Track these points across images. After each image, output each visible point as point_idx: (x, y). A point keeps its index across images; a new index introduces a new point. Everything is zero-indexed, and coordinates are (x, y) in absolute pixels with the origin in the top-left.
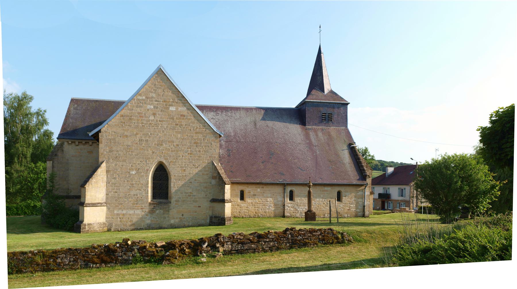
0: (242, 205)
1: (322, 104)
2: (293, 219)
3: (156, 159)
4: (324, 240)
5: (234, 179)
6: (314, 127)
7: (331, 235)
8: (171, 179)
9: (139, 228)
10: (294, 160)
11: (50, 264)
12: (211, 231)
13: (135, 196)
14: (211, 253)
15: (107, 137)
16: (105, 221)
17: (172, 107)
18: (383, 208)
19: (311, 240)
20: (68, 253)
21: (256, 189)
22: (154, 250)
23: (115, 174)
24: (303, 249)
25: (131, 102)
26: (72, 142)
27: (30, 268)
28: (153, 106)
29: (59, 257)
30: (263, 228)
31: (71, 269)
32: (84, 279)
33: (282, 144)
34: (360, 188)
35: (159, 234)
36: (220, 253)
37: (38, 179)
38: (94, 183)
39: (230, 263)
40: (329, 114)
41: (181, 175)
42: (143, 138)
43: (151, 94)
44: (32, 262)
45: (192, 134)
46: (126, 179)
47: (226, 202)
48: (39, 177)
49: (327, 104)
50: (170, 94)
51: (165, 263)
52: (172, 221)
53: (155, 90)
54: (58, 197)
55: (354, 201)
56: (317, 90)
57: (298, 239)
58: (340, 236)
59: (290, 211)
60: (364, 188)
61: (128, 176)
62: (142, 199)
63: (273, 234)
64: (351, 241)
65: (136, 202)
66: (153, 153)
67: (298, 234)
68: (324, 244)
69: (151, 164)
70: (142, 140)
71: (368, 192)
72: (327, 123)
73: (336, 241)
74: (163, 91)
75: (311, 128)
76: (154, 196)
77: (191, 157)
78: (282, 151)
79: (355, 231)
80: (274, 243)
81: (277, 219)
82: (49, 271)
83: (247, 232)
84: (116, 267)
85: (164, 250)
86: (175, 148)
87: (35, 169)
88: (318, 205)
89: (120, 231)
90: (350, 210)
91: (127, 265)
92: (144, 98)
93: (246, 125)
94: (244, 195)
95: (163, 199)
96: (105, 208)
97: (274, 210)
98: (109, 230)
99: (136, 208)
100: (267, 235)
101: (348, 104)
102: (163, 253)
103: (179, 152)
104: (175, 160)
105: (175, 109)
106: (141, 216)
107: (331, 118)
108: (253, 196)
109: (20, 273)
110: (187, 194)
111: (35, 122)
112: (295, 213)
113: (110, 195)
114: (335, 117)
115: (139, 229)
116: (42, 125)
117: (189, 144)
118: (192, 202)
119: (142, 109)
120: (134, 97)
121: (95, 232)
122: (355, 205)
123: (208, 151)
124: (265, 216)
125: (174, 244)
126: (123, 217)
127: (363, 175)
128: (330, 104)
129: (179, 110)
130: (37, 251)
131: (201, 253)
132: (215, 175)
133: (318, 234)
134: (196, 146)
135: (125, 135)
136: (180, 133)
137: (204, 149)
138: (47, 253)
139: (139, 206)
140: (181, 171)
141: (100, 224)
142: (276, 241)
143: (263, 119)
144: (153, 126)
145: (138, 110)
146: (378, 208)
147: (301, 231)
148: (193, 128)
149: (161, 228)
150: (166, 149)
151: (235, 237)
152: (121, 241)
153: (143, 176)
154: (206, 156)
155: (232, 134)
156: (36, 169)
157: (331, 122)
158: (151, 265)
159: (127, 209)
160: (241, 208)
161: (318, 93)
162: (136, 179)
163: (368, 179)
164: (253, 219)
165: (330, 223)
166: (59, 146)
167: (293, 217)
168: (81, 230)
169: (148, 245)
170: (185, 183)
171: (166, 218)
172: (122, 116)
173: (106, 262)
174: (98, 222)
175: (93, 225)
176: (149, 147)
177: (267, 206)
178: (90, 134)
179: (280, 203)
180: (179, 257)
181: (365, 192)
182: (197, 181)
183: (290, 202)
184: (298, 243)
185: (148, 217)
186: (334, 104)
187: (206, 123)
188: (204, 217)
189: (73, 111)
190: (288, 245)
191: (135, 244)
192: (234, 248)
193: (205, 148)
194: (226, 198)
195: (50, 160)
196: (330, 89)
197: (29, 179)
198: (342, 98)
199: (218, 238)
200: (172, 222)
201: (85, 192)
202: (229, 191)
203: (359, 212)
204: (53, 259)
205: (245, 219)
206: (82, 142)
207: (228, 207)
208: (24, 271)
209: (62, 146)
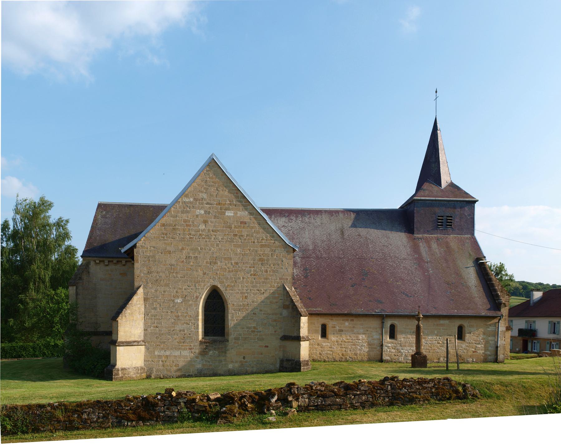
0: (324, 344)
1: (438, 202)
5: (312, 309)
9: (187, 374)
11: (74, 420)
14: (283, 410)
15: (145, 254)
16: (143, 365)
17: (229, 212)
18: (525, 350)
19: (420, 394)
22: (206, 404)
23: (155, 303)
24: (409, 406)
25: (174, 206)
26: (100, 261)
28: (203, 211)
29: (85, 412)
30: (353, 375)
31: (101, 427)
33: (380, 260)
34: (491, 321)
37: (59, 310)
40: (448, 217)
44: (52, 418)
45: (256, 248)
46: (170, 310)
47: (302, 340)
48: (60, 308)
50: (226, 193)
51: (220, 422)
52: (230, 366)
53: (207, 189)
54: (83, 334)
55: (482, 339)
58: (460, 389)
59: (390, 353)
60: (498, 321)
61: (171, 305)
62: (191, 337)
63: (366, 384)
64: (476, 397)
65: (183, 340)
66: (204, 274)
68: (439, 400)
69: (202, 289)
70: (189, 257)
71: (503, 327)
72: (444, 230)
73: (455, 395)
74: (217, 190)
75: (422, 237)
76: (206, 332)
77: (255, 279)
79: (483, 381)
80: (368, 398)
84: (157, 427)
86: (233, 267)
88: (430, 345)
90: (476, 352)
91: (171, 423)
92: (192, 200)
96: (143, 348)
97: (368, 351)
98: (148, 377)
100: (358, 386)
101: (475, 202)
102: (218, 408)
103: (239, 273)
104: (233, 284)
106: (189, 359)
107: (451, 222)
108: (339, 331)
110: (250, 329)
112: (398, 356)
113: (150, 331)
115: (187, 375)
116: (64, 240)
117: (252, 262)
118: (257, 340)
121: (131, 379)
122: (483, 346)
123: (278, 271)
124: (355, 359)
125: (232, 397)
129: (238, 215)
131: (268, 410)
133: (430, 386)
134: (262, 264)
135: (167, 250)
136: (239, 246)
137: (272, 267)
139: (187, 346)
141: (136, 368)
142: (370, 395)
143: (354, 225)
145: (184, 216)
146: (517, 349)
147: (406, 382)
148: (257, 240)
149: (215, 375)
151: (314, 388)
152: (163, 392)
153: (191, 305)
157: (450, 229)
159: (171, 349)
160: (322, 348)
161: (432, 187)
162: (182, 309)
164: (338, 363)
167: (395, 362)
170: (247, 315)
172: (163, 225)
173: (144, 420)
175: (128, 370)
176: (199, 266)
178: (123, 250)
179: (376, 342)
181: (498, 328)
182: (263, 312)
183: (390, 340)
184: (402, 398)
185: (198, 360)
186: (456, 203)
187: (275, 233)
188: (273, 360)
190: (387, 400)
191: (181, 395)
192: (312, 402)
194: (301, 335)
196: (449, 182)
198: (467, 194)
199: (291, 389)
202: (306, 325)
203: (490, 356)
204: (77, 414)
205: (328, 363)
208: (42, 429)
209: (88, 266)
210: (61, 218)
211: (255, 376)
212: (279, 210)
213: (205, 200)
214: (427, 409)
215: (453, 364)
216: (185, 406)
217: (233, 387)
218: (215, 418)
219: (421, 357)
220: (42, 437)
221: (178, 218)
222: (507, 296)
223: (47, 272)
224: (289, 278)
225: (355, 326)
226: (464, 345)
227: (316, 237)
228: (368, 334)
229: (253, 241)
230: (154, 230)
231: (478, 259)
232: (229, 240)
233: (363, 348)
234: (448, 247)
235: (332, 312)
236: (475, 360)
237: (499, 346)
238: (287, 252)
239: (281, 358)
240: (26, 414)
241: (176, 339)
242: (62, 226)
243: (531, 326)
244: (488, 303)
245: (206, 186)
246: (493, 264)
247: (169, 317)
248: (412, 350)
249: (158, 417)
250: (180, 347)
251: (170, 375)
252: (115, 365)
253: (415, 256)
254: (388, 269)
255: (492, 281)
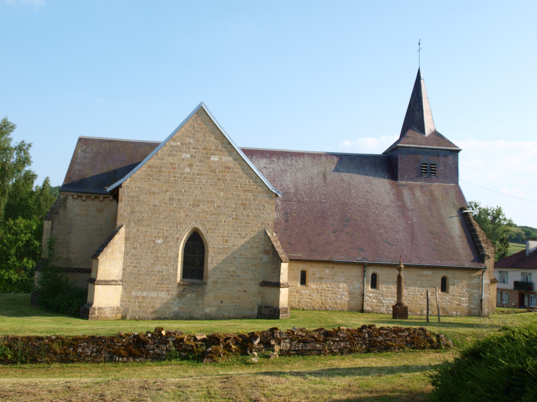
0: (303, 292)
1: (421, 150)
2: (376, 315)
3: (190, 224)
4: (412, 343)
5: (292, 255)
6: (409, 182)
7: (423, 337)
8: (208, 252)
9: (163, 317)
10: (379, 229)
11: (70, 354)
12: (264, 325)
13: (160, 273)
14: (264, 353)
15: (129, 194)
17: (214, 157)
18: (521, 305)
19: (395, 342)
20: (91, 342)
21: (324, 269)
22: (193, 344)
23: (135, 243)
24: (385, 353)
25: (162, 149)
26: (78, 196)
27: (46, 357)
28: (189, 155)
29: (80, 346)
30: (332, 324)
31: (94, 361)
32: (111, 374)
34: (474, 273)
35: (194, 325)
36: (275, 353)
37: (17, 240)
38: (109, 253)
39: (288, 366)
40: (431, 164)
41: (222, 247)
42: (175, 197)
43: (188, 139)
44: (49, 350)
47: (281, 286)
48: (18, 239)
49: (429, 150)
50: (212, 139)
51: (206, 361)
52: (207, 310)
53: (194, 135)
54: (59, 270)
55: (466, 292)
56: (414, 130)
57: (378, 340)
58: (434, 339)
59: (372, 303)
60: (481, 273)
61: (152, 245)
63: (345, 332)
64: (449, 347)
65: (161, 281)
66: (187, 216)
67: (378, 334)
68: (413, 349)
69: (183, 230)
70: (173, 198)
72: (429, 177)
73: (429, 345)
74: (204, 136)
76: (185, 274)
77: (236, 223)
78: (362, 216)
79: (457, 333)
80: (346, 344)
81: (352, 313)
82: (68, 363)
83: (311, 328)
84: (147, 363)
85: (205, 345)
87: (14, 227)
88: (412, 296)
89: (137, 319)
90: (460, 305)
91: (159, 361)
92: (179, 144)
93: (312, 178)
94: (307, 278)
95: (197, 279)
96: (120, 288)
97: (349, 301)
98: (124, 318)
99: (161, 289)
100: (337, 333)
101: (458, 151)
102: (204, 348)
103: (221, 216)
104: (214, 227)
105: (218, 159)
106: (166, 301)
109: (35, 363)
111: (15, 160)
113: (128, 271)
114: (440, 169)
116: (23, 165)
117: (234, 206)
119: (176, 158)
120: (166, 143)
121: (107, 319)
125: (218, 338)
126: (142, 300)
127: (480, 254)
128: (434, 151)
129: (223, 160)
130: (55, 337)
131: (251, 351)
132: (268, 248)
134: (244, 209)
136: (222, 190)
137: (253, 212)
138: (66, 340)
139: (164, 287)
140: (222, 242)
141: (112, 308)
142: (349, 342)
143: (337, 170)
144: (188, 181)
145: (171, 159)
146: (513, 304)
147: (383, 330)
148: (241, 185)
149: (191, 318)
150: (204, 211)
151: (295, 333)
152: (153, 331)
154: (256, 222)
155: (292, 191)
156: (16, 227)
157: (434, 177)
158: (189, 363)
159: (149, 290)
161: (416, 135)
162: (162, 250)
163: (487, 261)
164: (318, 312)
165: (428, 323)
166: (62, 201)
167: (376, 313)
168: (90, 316)
169: (186, 337)
171: (199, 305)
172: (150, 167)
173: (134, 356)
174: (110, 306)
175: (104, 310)
176: (182, 208)
177: (338, 294)
178: (109, 189)
179: (357, 291)
180: (223, 354)
181: (482, 280)
182: (243, 257)
184: (378, 346)
185: (175, 303)
186: (439, 151)
187: (258, 178)
189: (80, 154)
190: (364, 347)
191: (171, 335)
193: (255, 212)
194: (281, 281)
195: (49, 220)
196: (433, 130)
197: (5, 241)
199: (274, 333)
200: (206, 312)
201: (98, 265)
202: (287, 271)
203: (474, 309)
204: (73, 347)
205: (307, 312)
206: (90, 197)
207: (284, 293)
208: (40, 360)
210: (23, 142)
211: (233, 321)
212: (260, 150)
213: (192, 144)
214: (401, 356)
215: (433, 318)
216: (173, 344)
217: (216, 329)
218: (201, 357)
219: (402, 308)
220: (40, 367)
221: (164, 161)
222: (492, 248)
223: (3, 198)
224: (271, 223)
225: (336, 274)
226: (447, 297)
227: (298, 180)
228: (349, 282)
229: (236, 185)
230: (138, 172)
231: (462, 209)
232: (213, 183)
233: (344, 297)
234: (432, 194)
235: (312, 259)
236: (459, 314)
237: (483, 299)
238: (270, 197)
239: (260, 304)
240: (26, 345)
241: (154, 280)
242: (24, 150)
243: (527, 279)
244: (472, 254)
245: (194, 131)
246: (489, 208)
247: (148, 258)
248: (394, 301)
249: (147, 354)
250: (158, 288)
251: (145, 317)
252: (91, 304)
253: (399, 203)
254: (370, 216)
255: (476, 232)
